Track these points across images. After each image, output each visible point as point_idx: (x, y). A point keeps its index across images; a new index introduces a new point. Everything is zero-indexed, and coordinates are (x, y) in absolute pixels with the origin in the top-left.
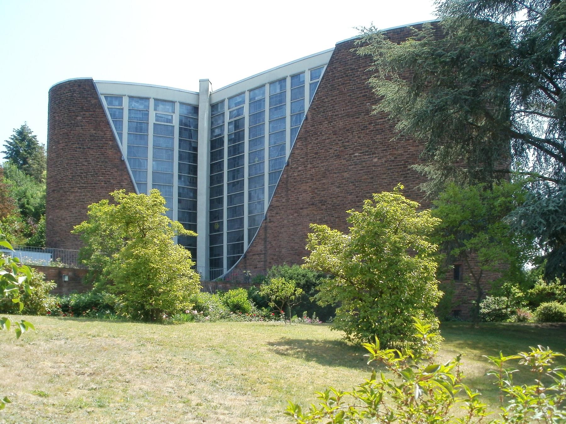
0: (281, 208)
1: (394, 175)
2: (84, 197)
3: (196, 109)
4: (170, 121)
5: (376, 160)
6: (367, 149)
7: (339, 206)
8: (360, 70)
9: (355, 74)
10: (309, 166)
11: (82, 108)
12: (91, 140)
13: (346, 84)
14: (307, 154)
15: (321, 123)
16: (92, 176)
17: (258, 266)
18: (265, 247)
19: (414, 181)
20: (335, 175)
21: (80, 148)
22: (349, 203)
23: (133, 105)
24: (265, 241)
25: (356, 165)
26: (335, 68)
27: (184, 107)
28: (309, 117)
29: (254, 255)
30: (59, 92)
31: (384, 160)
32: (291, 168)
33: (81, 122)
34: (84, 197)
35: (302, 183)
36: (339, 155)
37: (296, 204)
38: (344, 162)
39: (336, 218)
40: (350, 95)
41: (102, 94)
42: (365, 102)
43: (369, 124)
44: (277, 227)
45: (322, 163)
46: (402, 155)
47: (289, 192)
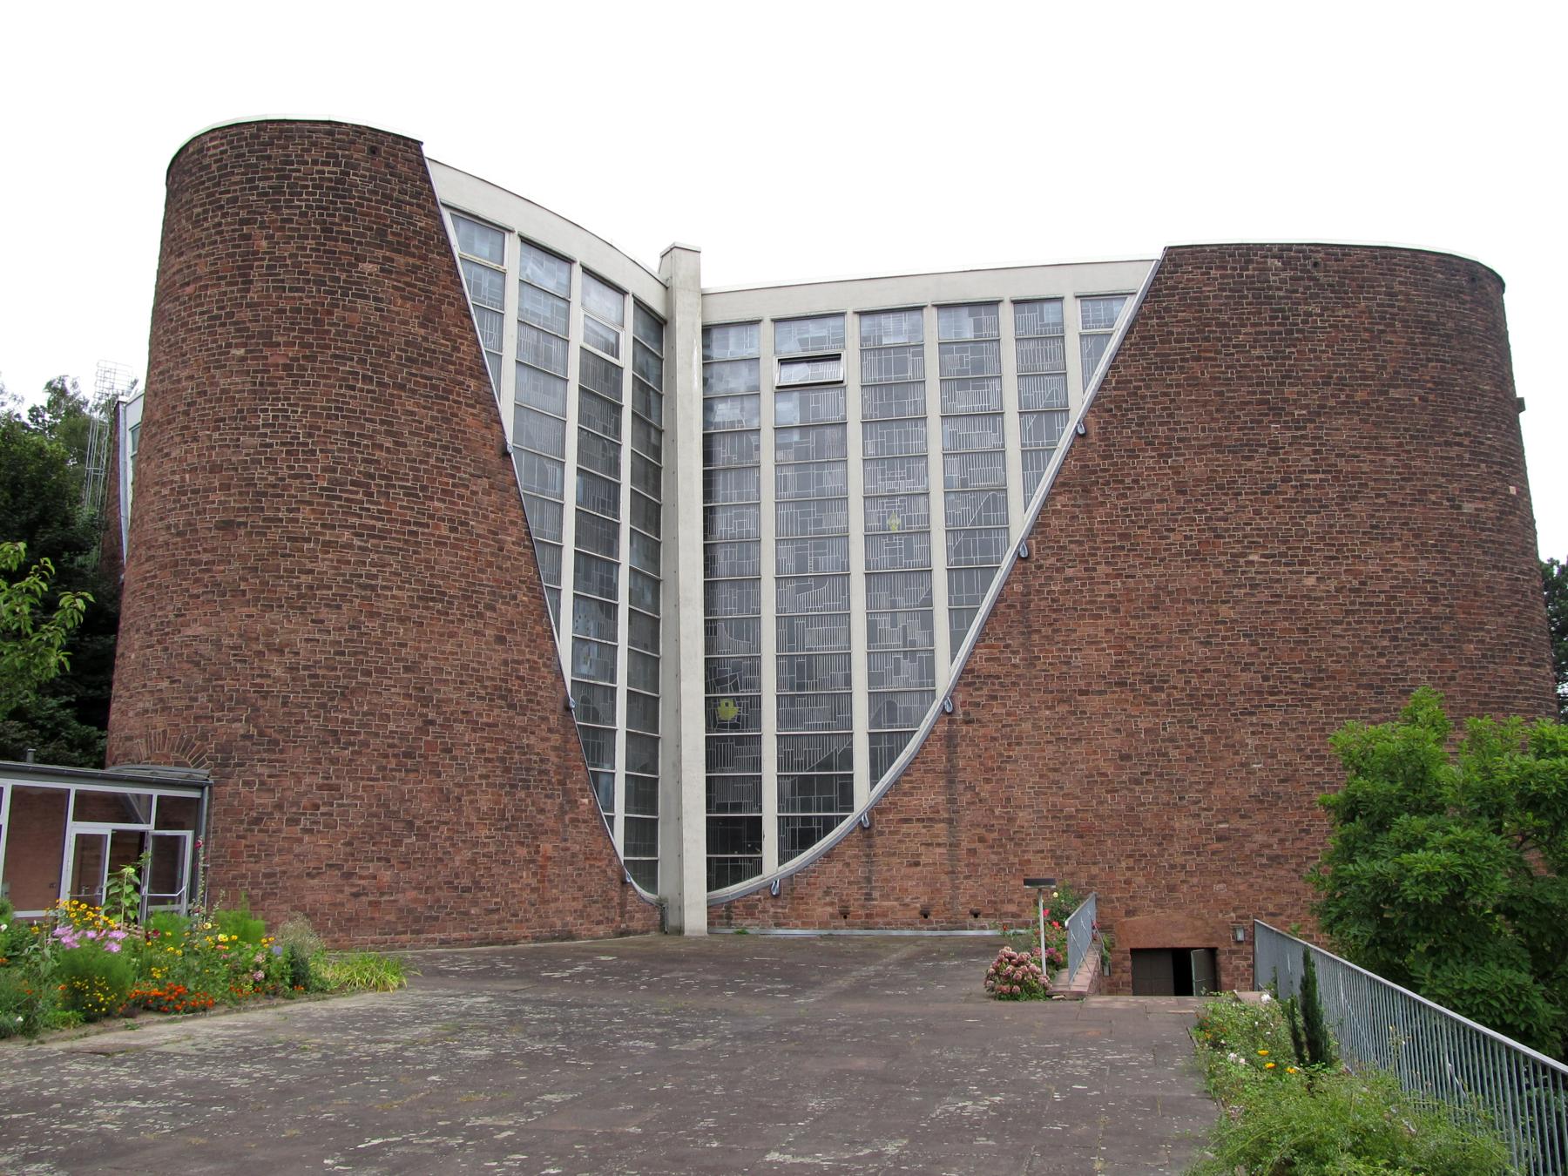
0: (1008, 681)
1: (1365, 629)
2: (374, 570)
4: (614, 350)
5: (1311, 581)
6: (1283, 548)
7: (1211, 697)
8: (1243, 330)
9: (1230, 339)
11: (382, 233)
12: (409, 359)
13: (1206, 359)
14: (1091, 534)
15: (1132, 453)
16: (410, 493)
17: (923, 860)
18: (952, 801)
19: (1416, 653)
20: (1190, 608)
22: (1242, 693)
23: (529, 271)
24: (951, 782)
26: (1167, 310)
28: (1094, 430)
29: (906, 821)
32: (1040, 567)
33: (377, 283)
34: (374, 570)
35: (1081, 617)
36: (1198, 553)
37: (1061, 677)
38: (1218, 574)
39: (1205, 732)
40: (1220, 394)
41: (445, 205)
42: (1266, 419)
43: (1284, 480)
44: (994, 739)
45: (1146, 565)
46: (1379, 578)
47: (1036, 637)
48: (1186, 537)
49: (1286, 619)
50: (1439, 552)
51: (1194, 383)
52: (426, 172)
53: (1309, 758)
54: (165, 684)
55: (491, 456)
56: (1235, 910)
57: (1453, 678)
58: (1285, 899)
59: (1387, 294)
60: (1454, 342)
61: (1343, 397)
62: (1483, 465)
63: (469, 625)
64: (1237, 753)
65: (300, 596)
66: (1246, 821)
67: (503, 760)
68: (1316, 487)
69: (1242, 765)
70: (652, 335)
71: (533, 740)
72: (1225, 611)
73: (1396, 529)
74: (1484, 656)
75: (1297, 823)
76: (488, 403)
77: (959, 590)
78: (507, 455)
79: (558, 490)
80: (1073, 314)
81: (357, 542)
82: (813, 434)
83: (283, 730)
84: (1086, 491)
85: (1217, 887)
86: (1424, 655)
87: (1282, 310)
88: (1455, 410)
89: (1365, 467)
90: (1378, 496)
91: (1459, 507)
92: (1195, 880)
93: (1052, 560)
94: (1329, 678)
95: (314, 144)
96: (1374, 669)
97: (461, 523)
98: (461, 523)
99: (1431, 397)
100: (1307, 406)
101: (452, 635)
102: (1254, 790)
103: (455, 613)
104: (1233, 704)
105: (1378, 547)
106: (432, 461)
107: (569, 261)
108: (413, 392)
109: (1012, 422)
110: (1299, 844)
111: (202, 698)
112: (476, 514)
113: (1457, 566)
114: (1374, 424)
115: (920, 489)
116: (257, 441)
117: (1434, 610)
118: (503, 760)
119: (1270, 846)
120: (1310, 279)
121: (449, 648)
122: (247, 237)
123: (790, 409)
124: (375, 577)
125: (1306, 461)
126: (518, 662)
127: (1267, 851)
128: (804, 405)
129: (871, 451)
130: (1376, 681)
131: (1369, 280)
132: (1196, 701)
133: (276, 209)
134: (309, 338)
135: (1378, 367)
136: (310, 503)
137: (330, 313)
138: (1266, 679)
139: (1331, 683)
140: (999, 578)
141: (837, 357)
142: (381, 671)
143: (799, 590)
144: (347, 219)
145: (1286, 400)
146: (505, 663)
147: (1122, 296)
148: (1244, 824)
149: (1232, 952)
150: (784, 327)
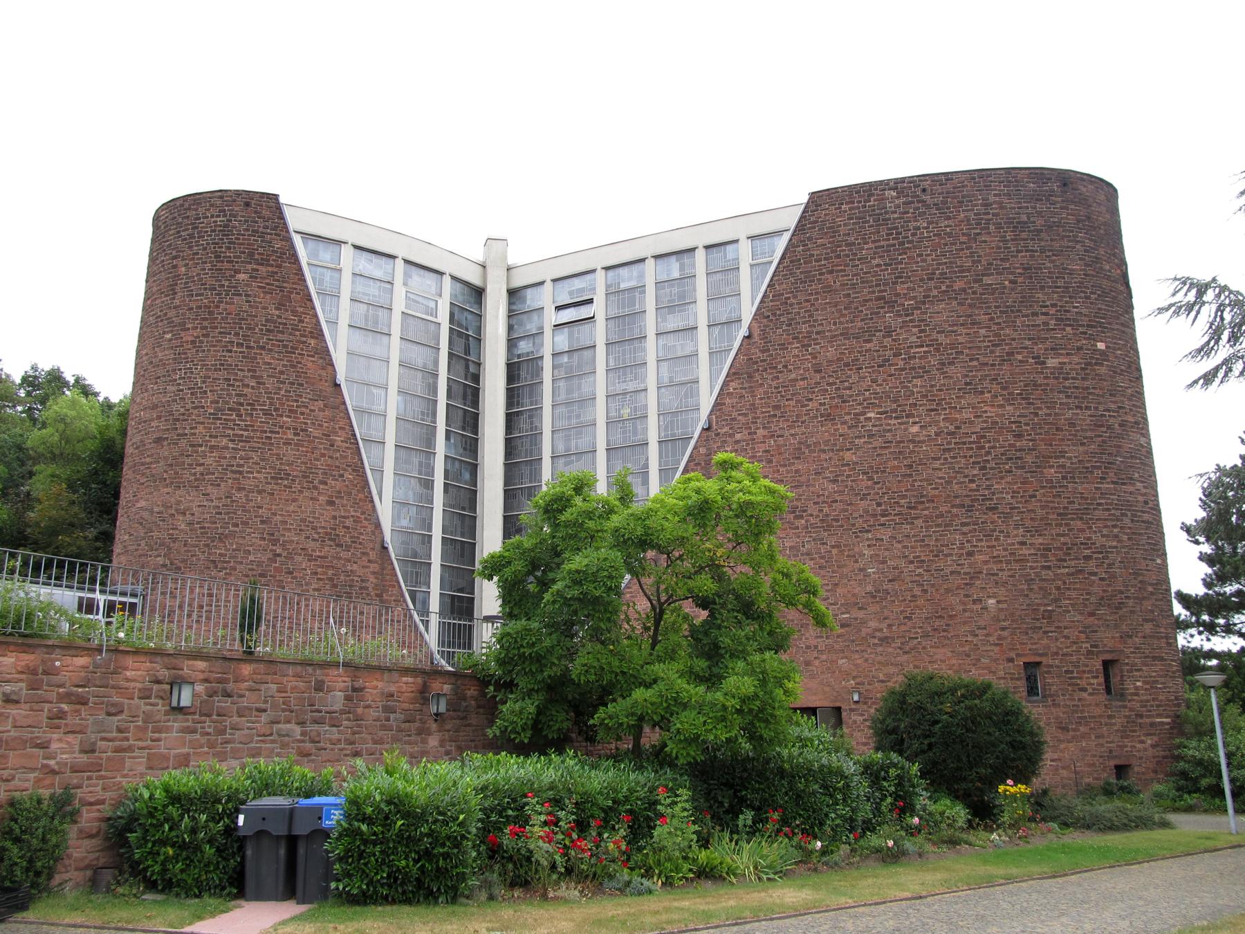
1: (958, 463)
2: (242, 462)
3: (478, 293)
5: (915, 429)
7: (837, 520)
10: (761, 432)
11: (251, 255)
12: (268, 330)
15: (783, 347)
19: (1002, 478)
20: (823, 456)
21: (240, 345)
23: (361, 267)
25: (871, 436)
26: (810, 239)
27: (458, 285)
28: (756, 333)
30: (191, 213)
31: (932, 431)
32: (717, 435)
33: (247, 285)
34: (242, 462)
36: (829, 415)
38: (843, 429)
39: (833, 547)
41: (306, 236)
46: (971, 423)
48: (821, 404)
49: (895, 459)
50: (1024, 399)
51: (829, 290)
52: (281, 213)
53: (912, 562)
54: (127, 537)
55: (327, 387)
56: (854, 678)
57: (1035, 496)
58: (892, 670)
59: (982, 205)
60: (1043, 235)
61: (944, 288)
62: (1068, 329)
63: (306, 494)
64: (856, 561)
65: (196, 480)
66: (863, 612)
67: (331, 579)
68: (920, 358)
69: (860, 570)
70: (472, 300)
71: (355, 567)
72: (848, 456)
73: (986, 384)
74: (1064, 478)
75: (902, 612)
76: (324, 355)
77: (667, 456)
78: (338, 386)
79: (382, 407)
80: (745, 249)
81: (231, 445)
82: (576, 355)
83: (184, 561)
84: (750, 376)
85: (840, 662)
86: (1009, 479)
87: (896, 228)
88: (1042, 288)
89: (961, 339)
90: (971, 360)
91: (1044, 363)
92: (824, 657)
93: (726, 429)
94: (928, 501)
95: (212, 205)
96: (965, 493)
97: (302, 430)
98: (302, 430)
99: (1020, 280)
100: (914, 298)
101: (294, 500)
102: (869, 588)
103: (296, 486)
104: (854, 525)
105: (971, 399)
106: (283, 392)
107: (393, 257)
108: (270, 350)
109: (703, 332)
110: (903, 628)
111: (143, 543)
112: (313, 424)
113: (1040, 408)
114: (970, 306)
115: (642, 386)
116: (175, 388)
117: (1018, 444)
118: (331, 579)
119: (881, 630)
120: (919, 202)
121: (291, 508)
122: (175, 267)
123: (563, 341)
124: (242, 466)
125: (914, 339)
126: (344, 517)
127: (878, 634)
128: (571, 336)
129: (612, 363)
130: (967, 502)
131: (968, 196)
132: (826, 524)
133: (190, 247)
134: (206, 323)
135: (974, 262)
136: (203, 423)
137: (218, 307)
138: (879, 505)
139: (931, 505)
140: (693, 442)
141: (590, 301)
142: (245, 523)
143: (566, 464)
144: (229, 248)
145: (898, 295)
146: (335, 518)
147: (779, 233)
148: (861, 614)
149: (852, 710)
150: (560, 284)
